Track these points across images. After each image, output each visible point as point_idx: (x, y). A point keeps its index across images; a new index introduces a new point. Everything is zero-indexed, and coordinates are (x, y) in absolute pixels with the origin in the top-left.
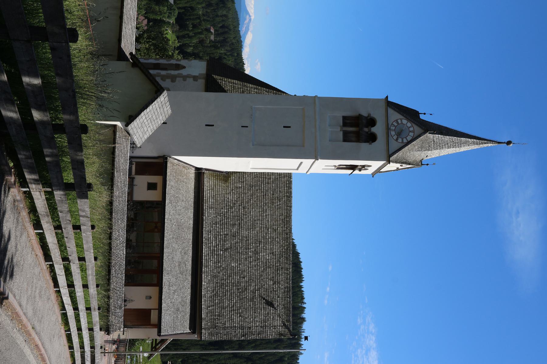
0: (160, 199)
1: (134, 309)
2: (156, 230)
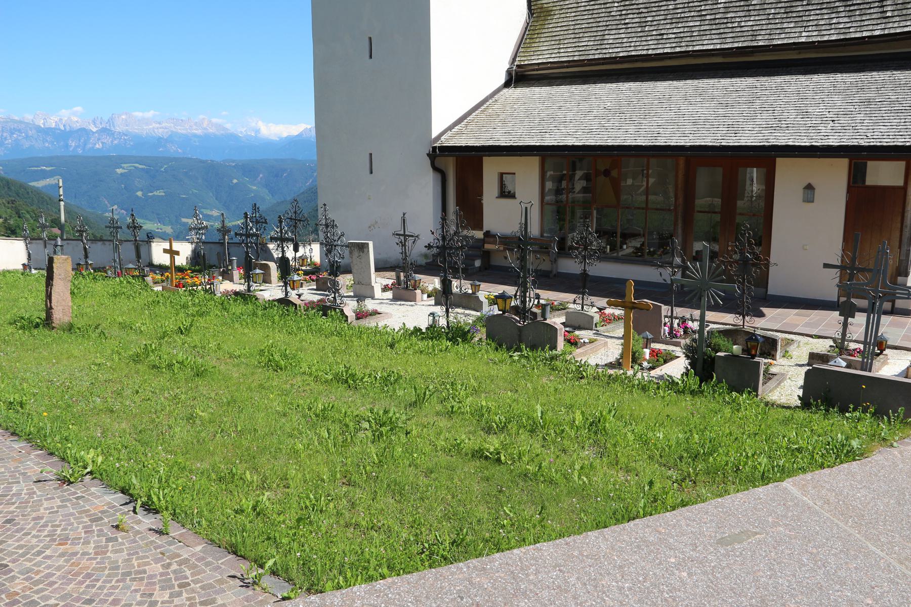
0: (534, 162)
1: (846, 239)
2: (614, 173)
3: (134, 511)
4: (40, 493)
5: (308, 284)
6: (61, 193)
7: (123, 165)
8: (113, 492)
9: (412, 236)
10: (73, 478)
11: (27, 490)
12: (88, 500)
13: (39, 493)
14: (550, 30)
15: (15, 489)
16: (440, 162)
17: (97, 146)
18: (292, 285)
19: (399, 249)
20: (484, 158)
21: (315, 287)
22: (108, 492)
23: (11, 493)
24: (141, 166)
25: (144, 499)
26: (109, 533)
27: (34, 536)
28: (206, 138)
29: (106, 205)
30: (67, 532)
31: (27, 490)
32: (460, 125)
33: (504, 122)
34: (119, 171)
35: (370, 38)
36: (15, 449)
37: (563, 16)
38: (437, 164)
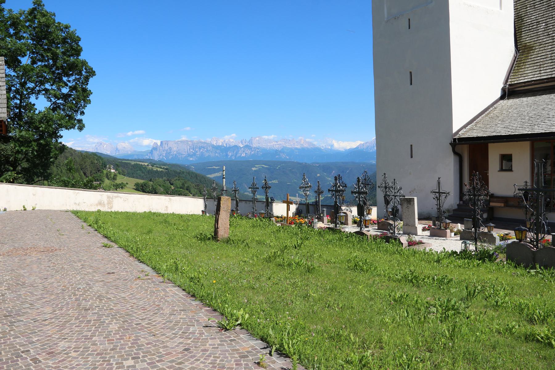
0: (527, 145)
3: (270, 354)
4: (207, 334)
5: (372, 226)
6: (224, 174)
7: (256, 166)
8: (255, 339)
9: (445, 193)
10: (228, 326)
11: (199, 331)
12: (238, 343)
13: (206, 334)
14: (532, 59)
15: (191, 329)
16: (458, 148)
17: (243, 155)
18: (365, 223)
19: (435, 202)
20: (489, 144)
21: (377, 228)
22: (252, 339)
23: (189, 332)
24: (265, 166)
25: (278, 346)
26: (253, 367)
27: (202, 362)
28: (303, 150)
29: (246, 188)
30: (224, 363)
31: (199, 331)
32: (471, 125)
33: (503, 121)
34: (254, 169)
35: (411, 73)
36: (193, 305)
37: (542, 49)
38: (456, 150)
